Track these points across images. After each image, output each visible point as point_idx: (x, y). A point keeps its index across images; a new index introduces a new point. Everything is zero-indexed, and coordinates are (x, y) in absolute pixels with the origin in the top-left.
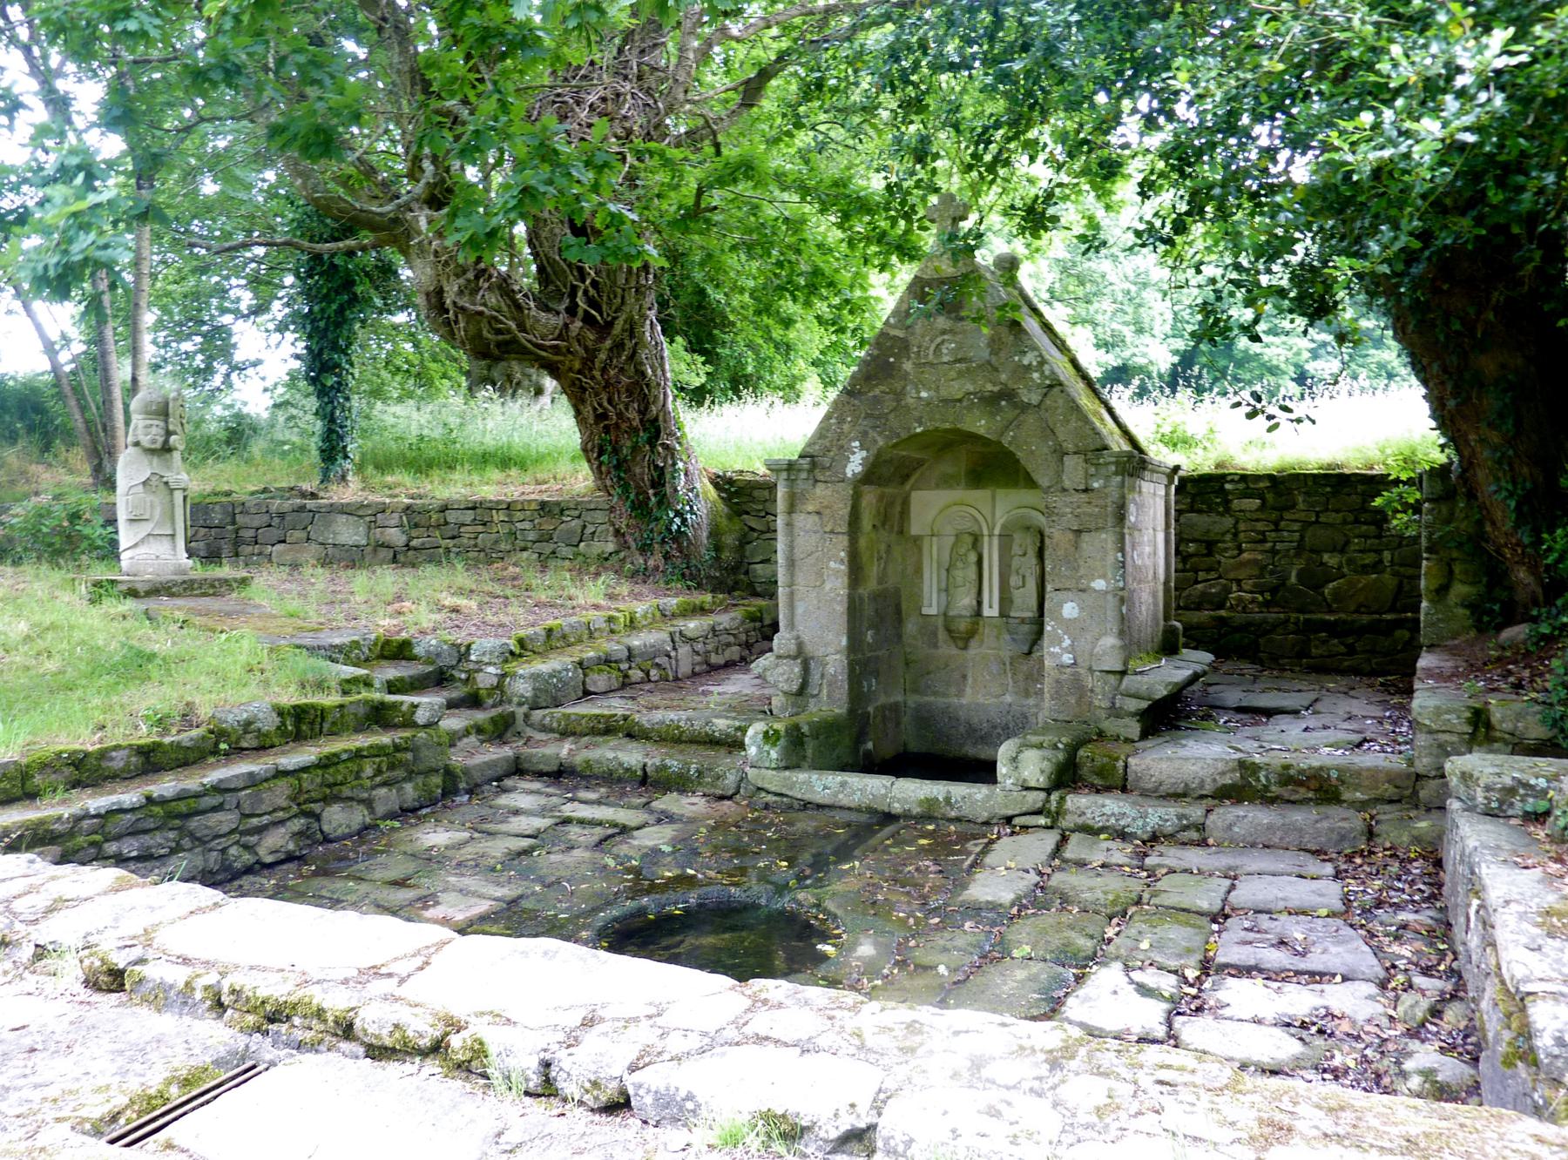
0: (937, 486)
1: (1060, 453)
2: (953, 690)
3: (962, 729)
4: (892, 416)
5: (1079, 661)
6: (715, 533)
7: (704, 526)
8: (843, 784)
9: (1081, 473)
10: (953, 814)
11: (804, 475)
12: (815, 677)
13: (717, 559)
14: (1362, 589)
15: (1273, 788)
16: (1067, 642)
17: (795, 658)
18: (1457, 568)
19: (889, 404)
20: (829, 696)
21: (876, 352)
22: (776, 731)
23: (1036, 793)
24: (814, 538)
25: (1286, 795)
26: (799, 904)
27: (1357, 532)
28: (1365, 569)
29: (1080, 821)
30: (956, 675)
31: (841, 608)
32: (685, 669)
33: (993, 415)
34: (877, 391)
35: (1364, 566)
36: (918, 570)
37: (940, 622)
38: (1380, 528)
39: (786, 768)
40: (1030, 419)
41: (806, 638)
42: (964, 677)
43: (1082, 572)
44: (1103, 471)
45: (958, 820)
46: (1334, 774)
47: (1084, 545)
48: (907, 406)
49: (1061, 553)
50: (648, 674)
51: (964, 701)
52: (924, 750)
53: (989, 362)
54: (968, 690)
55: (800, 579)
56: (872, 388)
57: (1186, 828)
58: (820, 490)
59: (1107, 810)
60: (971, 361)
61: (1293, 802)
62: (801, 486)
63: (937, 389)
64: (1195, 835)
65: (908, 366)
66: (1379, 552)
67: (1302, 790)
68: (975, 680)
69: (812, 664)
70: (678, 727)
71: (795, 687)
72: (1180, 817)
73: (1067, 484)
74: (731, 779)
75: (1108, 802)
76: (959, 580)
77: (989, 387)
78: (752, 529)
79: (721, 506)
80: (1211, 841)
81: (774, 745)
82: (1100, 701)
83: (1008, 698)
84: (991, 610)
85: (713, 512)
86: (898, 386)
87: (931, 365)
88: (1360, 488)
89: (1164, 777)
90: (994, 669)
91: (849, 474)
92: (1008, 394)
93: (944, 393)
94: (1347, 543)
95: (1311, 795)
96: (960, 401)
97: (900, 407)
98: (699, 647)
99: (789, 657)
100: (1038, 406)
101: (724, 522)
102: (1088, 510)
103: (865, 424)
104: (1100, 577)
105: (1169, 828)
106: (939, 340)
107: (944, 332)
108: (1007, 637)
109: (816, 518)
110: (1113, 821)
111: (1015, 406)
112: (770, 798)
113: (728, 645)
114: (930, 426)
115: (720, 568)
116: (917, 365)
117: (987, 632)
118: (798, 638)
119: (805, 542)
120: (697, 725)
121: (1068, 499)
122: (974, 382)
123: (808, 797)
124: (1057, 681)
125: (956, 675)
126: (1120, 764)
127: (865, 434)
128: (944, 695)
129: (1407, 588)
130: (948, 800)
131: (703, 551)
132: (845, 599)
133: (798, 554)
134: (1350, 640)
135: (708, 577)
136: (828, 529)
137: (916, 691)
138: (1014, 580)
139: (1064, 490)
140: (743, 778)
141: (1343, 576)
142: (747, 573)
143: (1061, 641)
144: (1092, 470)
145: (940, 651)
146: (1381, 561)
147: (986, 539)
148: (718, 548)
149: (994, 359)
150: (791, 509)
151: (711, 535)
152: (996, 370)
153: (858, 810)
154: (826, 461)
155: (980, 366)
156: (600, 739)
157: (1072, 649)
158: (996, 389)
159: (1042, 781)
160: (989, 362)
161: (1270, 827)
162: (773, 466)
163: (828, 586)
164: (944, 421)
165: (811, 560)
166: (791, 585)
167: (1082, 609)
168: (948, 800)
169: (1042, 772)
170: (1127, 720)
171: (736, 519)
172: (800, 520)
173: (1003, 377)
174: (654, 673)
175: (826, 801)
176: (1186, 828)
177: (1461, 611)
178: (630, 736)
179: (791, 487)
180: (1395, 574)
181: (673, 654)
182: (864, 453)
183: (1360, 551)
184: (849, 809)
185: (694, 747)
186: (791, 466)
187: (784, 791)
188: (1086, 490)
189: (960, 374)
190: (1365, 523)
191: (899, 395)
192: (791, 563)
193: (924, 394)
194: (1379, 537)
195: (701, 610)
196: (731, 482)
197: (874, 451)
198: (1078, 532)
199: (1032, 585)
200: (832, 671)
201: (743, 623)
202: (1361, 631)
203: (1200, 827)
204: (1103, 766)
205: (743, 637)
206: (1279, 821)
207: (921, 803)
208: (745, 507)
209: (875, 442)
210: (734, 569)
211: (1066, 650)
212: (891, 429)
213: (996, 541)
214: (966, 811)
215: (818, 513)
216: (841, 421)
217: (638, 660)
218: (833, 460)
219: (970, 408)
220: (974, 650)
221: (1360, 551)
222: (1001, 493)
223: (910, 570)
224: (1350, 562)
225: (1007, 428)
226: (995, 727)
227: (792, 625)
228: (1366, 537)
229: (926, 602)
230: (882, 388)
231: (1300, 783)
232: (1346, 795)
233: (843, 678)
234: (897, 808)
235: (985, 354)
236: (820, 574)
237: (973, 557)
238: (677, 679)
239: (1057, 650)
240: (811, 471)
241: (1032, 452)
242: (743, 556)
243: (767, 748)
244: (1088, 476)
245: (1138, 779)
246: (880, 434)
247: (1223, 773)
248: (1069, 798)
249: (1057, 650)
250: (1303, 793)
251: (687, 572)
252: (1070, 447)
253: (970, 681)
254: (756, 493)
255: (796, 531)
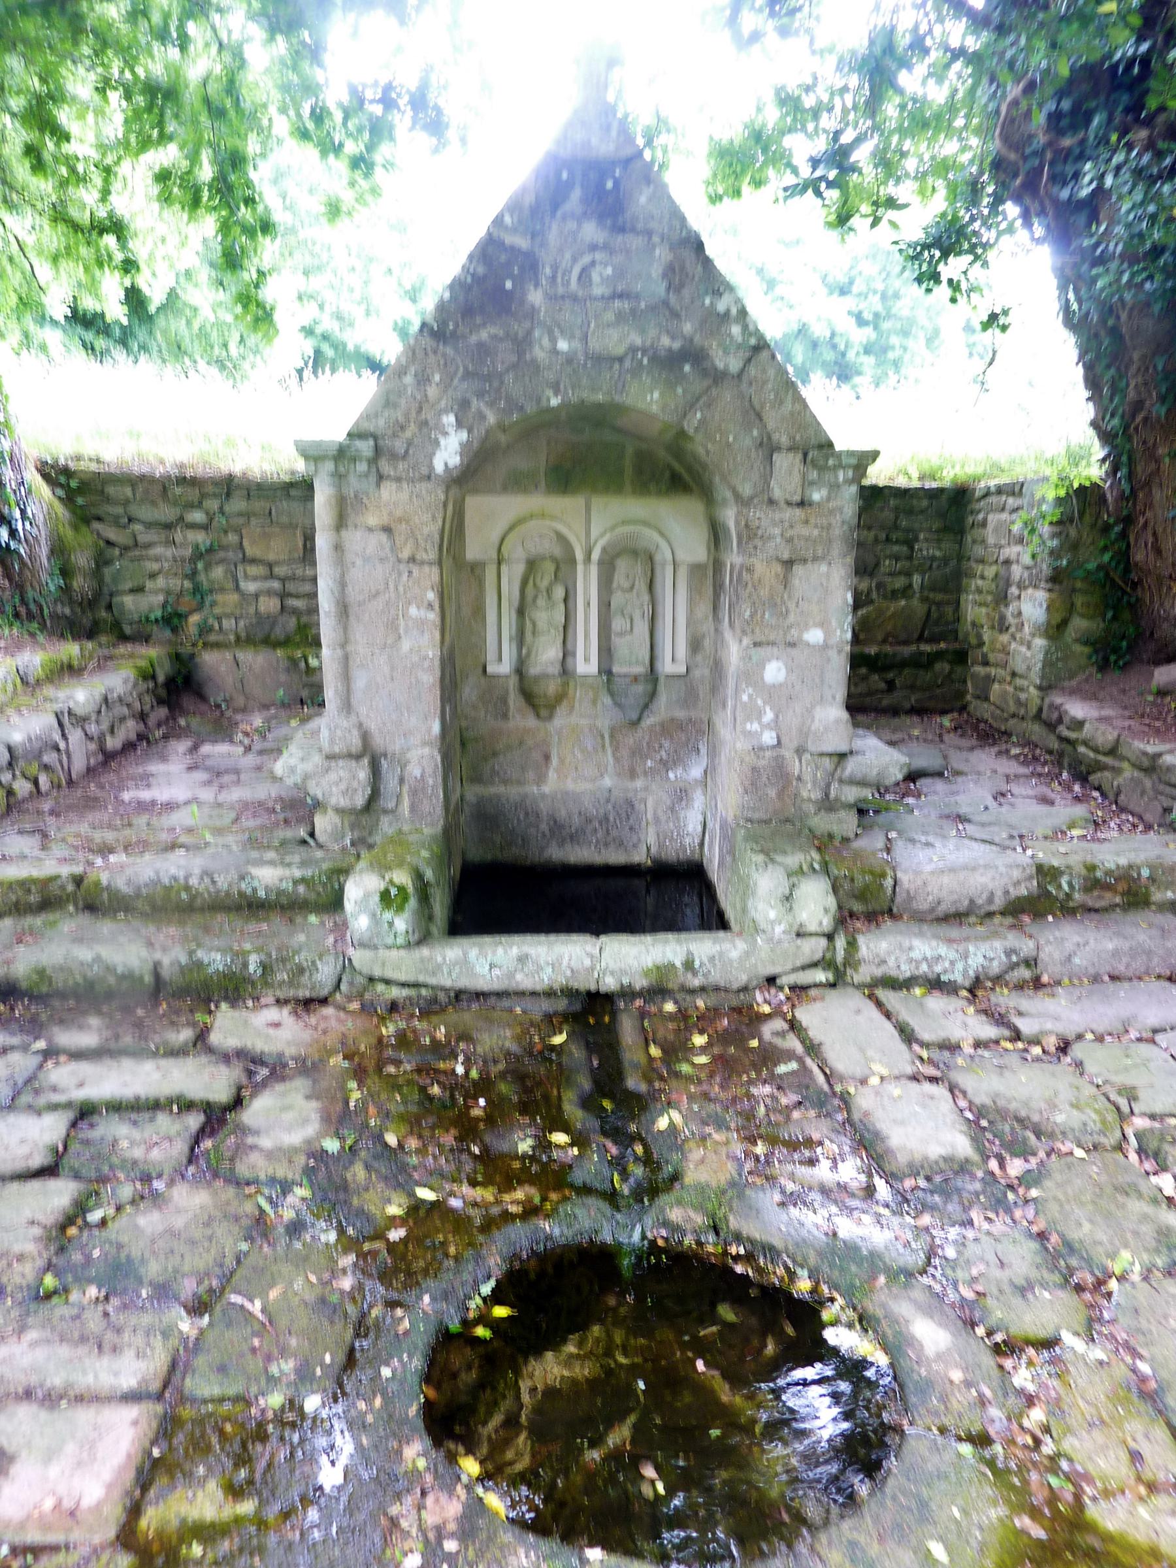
0: (505, 489)
1: (769, 448)
2: (531, 775)
3: (544, 827)
4: (509, 378)
5: (784, 740)
6: (58, 550)
7: (43, 542)
8: (522, 959)
9: (796, 478)
10: (696, 982)
11: (362, 467)
12: (390, 783)
13: (66, 590)
14: (890, 618)
15: (1077, 896)
16: (769, 716)
17: (358, 757)
18: (1079, 600)
19: (505, 356)
20: (413, 808)
21: (481, 270)
22: (401, 889)
23: (813, 940)
24: (380, 571)
25: (1090, 903)
26: (675, 1228)
27: (888, 552)
28: (895, 595)
29: (879, 972)
30: (536, 756)
31: (429, 678)
32: (79, 765)
33: (670, 386)
34: (484, 335)
35: (894, 592)
36: (479, 611)
37: (513, 682)
38: (912, 548)
39: (420, 943)
40: (726, 396)
41: (372, 726)
42: (547, 758)
43: (792, 618)
44: (828, 476)
45: (703, 989)
46: (1145, 873)
47: (796, 582)
48: (534, 361)
49: (764, 593)
50: (36, 782)
51: (546, 789)
52: (489, 857)
53: (666, 303)
54: (552, 775)
55: (359, 634)
56: (475, 328)
57: (1013, 966)
58: (388, 491)
59: (916, 955)
60: (638, 297)
61: (1096, 911)
62: (354, 484)
63: (585, 338)
64: (1026, 973)
65: (535, 297)
66: (909, 574)
67: (1108, 895)
68: (562, 761)
69: (384, 764)
70: (187, 888)
71: (360, 801)
72: (1009, 953)
73: (777, 493)
74: (325, 973)
75: (916, 943)
76: (542, 624)
77: (666, 341)
78: (109, 543)
79: (60, 509)
80: (1045, 979)
81: (400, 909)
82: (810, 792)
83: (608, 782)
84: (586, 664)
85: (50, 515)
86: (519, 329)
87: (575, 298)
88: (892, 502)
89: (944, 894)
90: (589, 744)
91: (439, 468)
92: (694, 355)
93: (595, 345)
94: (877, 565)
95: (1118, 900)
96: (621, 360)
97: (524, 365)
98: (93, 729)
99: (350, 756)
100: (740, 375)
101: (68, 533)
102: (805, 531)
103: (462, 388)
104: (816, 625)
105: (995, 968)
106: (587, 259)
107: (593, 248)
108: (608, 700)
109: (383, 537)
110: (924, 968)
111: (704, 373)
112: (395, 993)
113: (123, 719)
114: (573, 397)
115: (71, 602)
116: (552, 298)
117: (579, 694)
118: (361, 725)
119: (362, 577)
120: (223, 882)
121: (777, 516)
122: (643, 332)
123: (464, 982)
124: (754, 769)
125: (536, 756)
126: (889, 882)
127: (464, 404)
128: (519, 783)
129: (934, 615)
130: (689, 965)
131: (44, 577)
132: (437, 663)
133: (353, 594)
134: (891, 675)
135: (54, 616)
136: (405, 554)
137: (477, 779)
138: (618, 624)
139: (771, 502)
140: (347, 965)
141: (872, 602)
142: (109, 607)
143: (760, 714)
144: (814, 475)
145: (511, 724)
146: (910, 586)
147: (580, 568)
148: (66, 572)
149: (673, 299)
150: (341, 522)
151: (52, 552)
152: (675, 315)
153: (550, 994)
154: (399, 446)
155: (652, 308)
156: (38, 921)
157: (776, 724)
158: (676, 345)
159: (827, 923)
160: (666, 303)
161: (1116, 953)
162: (312, 453)
163: (406, 645)
164: (593, 389)
165: (379, 604)
166: (344, 644)
167: (790, 670)
168: (689, 965)
169: (826, 910)
170: (843, 814)
171: (84, 529)
172: (354, 539)
173: (688, 328)
174: (43, 780)
175: (496, 986)
176: (1013, 966)
177: (1078, 648)
178: (92, 907)
179: (339, 488)
180: (924, 599)
181: (62, 745)
182: (464, 435)
183: (890, 574)
184: (534, 994)
185: (220, 917)
186: (342, 454)
187: (421, 979)
188: (802, 504)
189: (620, 317)
190: (897, 542)
191: (522, 344)
192: (344, 610)
193: (563, 345)
194: (910, 558)
195: (69, 671)
196: (66, 472)
197: (480, 431)
198: (789, 564)
199: (642, 628)
200: (417, 772)
201: (135, 685)
202: (903, 664)
203: (1030, 962)
204: (867, 887)
205: (137, 705)
206: (1125, 945)
207: (646, 973)
208: (94, 511)
209: (482, 417)
210: (92, 604)
211: (768, 726)
212: (509, 399)
213: (594, 570)
214: (716, 976)
215: (387, 530)
216: (423, 380)
217: (22, 763)
218: (410, 444)
219: (637, 370)
220: (560, 720)
221: (890, 574)
222: (598, 502)
223: (466, 611)
224: (880, 586)
225: (691, 406)
226: (589, 821)
227: (347, 706)
228: (897, 559)
229: (491, 655)
230: (493, 330)
231: (1107, 887)
232: (1157, 896)
233: (434, 782)
234: (610, 984)
235: (660, 289)
236: (392, 626)
237: (559, 592)
238: (70, 782)
239: (755, 727)
240: (374, 460)
241: (728, 445)
242: (101, 582)
243: (388, 915)
244: (806, 484)
245: (910, 898)
246: (491, 404)
247: (1017, 883)
248: (861, 940)
249: (755, 727)
250: (1109, 898)
251: (23, 611)
252: (784, 440)
253: (555, 761)
254: (111, 490)
255: (349, 557)
